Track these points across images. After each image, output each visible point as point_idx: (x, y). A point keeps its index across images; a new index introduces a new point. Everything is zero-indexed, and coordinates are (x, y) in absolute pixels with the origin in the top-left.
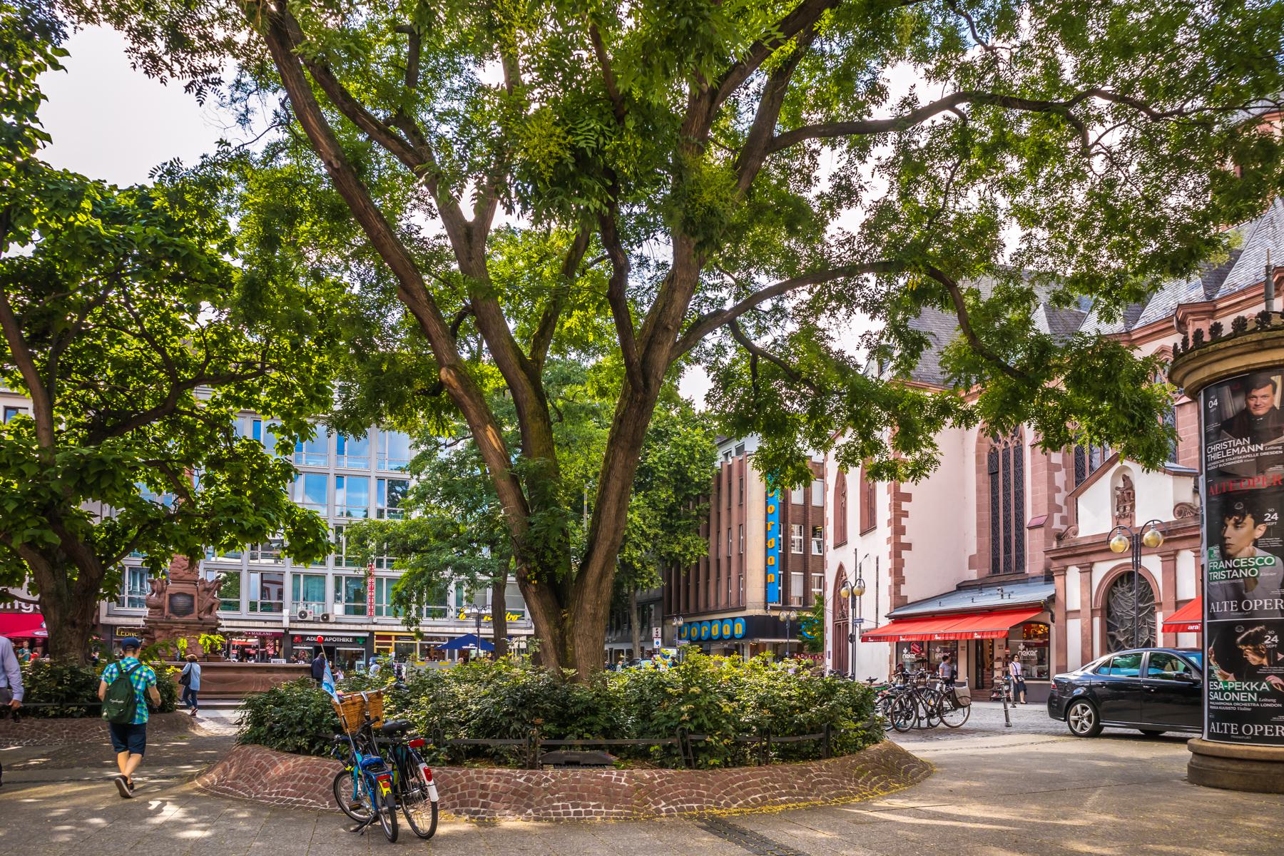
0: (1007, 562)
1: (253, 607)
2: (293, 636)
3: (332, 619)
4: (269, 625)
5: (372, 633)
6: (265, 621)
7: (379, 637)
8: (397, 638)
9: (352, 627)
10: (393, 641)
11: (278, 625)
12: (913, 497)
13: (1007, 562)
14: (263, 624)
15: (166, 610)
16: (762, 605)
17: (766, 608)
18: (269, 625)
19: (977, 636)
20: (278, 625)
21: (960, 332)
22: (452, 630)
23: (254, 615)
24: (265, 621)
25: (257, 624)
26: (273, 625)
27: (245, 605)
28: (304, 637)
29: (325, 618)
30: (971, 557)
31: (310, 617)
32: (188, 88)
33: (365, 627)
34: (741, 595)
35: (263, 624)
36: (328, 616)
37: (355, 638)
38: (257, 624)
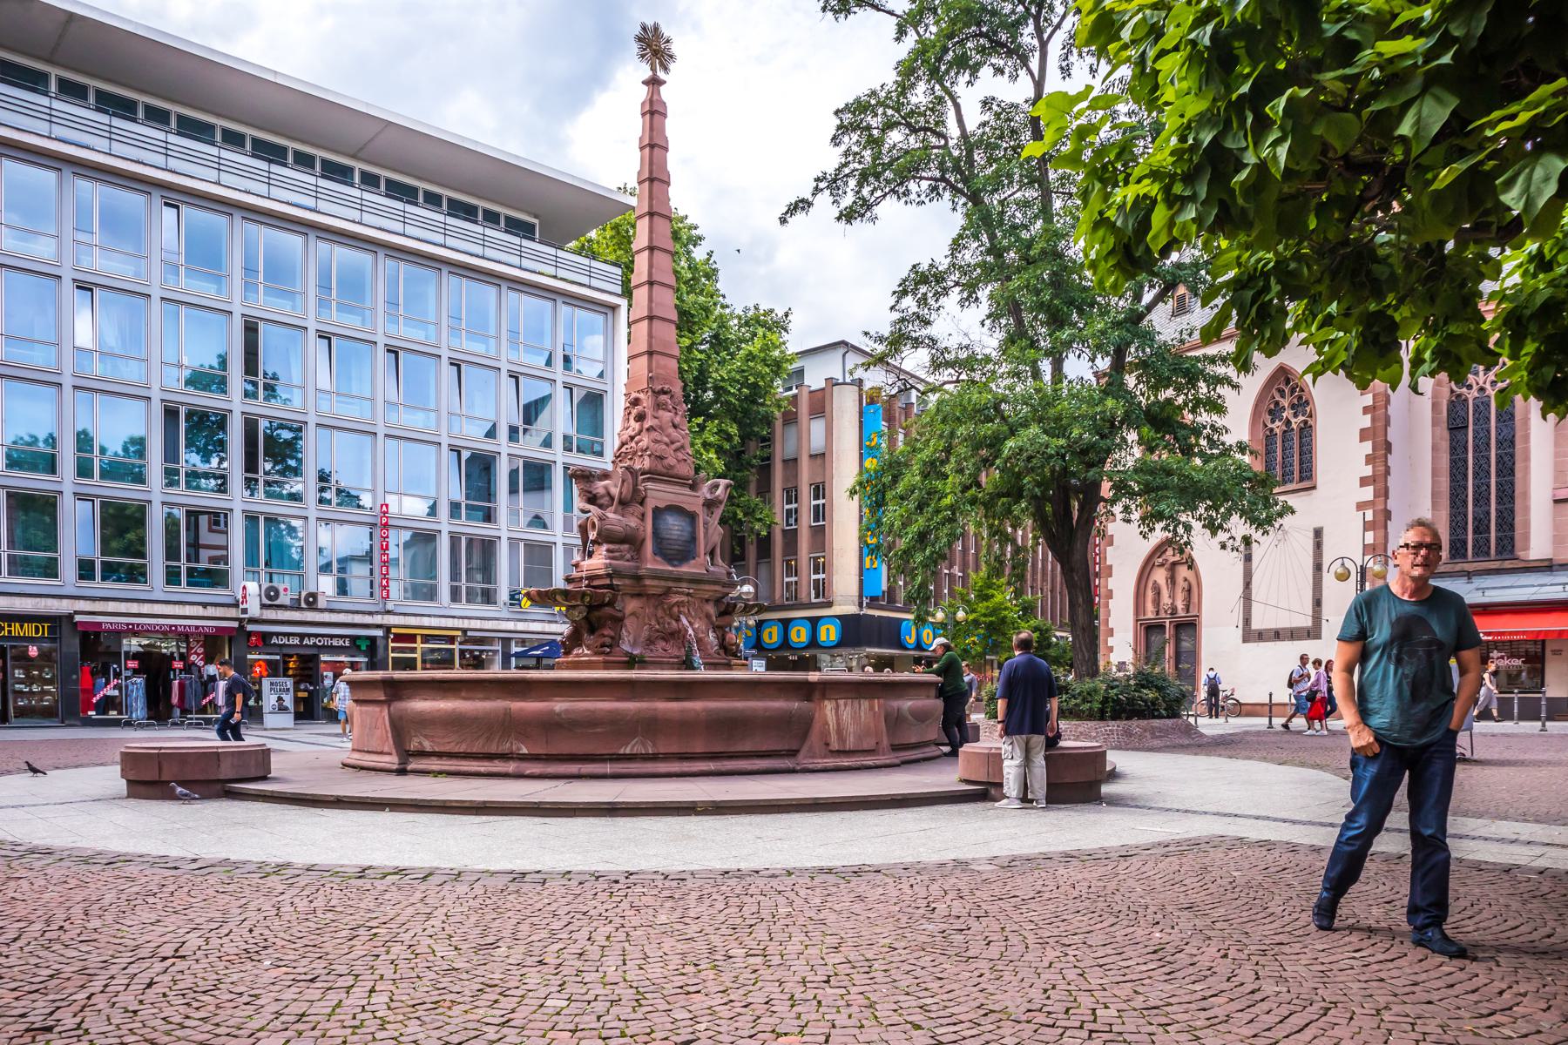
0: (1481, 527)
1: (86, 570)
2: (250, 634)
3: (321, 603)
4: (211, 611)
5: (388, 629)
6: (205, 605)
7: (399, 638)
8: (426, 639)
9: (358, 619)
10: (419, 645)
11: (232, 613)
12: (1318, 525)
13: (1481, 527)
14: (199, 611)
15: (649, 546)
16: (856, 599)
17: (861, 605)
18: (211, 611)
19: (921, 669)
20: (232, 613)
21: (865, 704)
22: (510, 626)
23: (88, 587)
24: (205, 605)
25: (188, 610)
26: (219, 612)
27: (68, 569)
28: (265, 637)
29: (312, 602)
30: (1362, 430)
31: (284, 599)
32: (1361, 506)
33: (378, 619)
34: (821, 588)
35: (199, 611)
36: (314, 595)
37: (354, 639)
38: (188, 610)
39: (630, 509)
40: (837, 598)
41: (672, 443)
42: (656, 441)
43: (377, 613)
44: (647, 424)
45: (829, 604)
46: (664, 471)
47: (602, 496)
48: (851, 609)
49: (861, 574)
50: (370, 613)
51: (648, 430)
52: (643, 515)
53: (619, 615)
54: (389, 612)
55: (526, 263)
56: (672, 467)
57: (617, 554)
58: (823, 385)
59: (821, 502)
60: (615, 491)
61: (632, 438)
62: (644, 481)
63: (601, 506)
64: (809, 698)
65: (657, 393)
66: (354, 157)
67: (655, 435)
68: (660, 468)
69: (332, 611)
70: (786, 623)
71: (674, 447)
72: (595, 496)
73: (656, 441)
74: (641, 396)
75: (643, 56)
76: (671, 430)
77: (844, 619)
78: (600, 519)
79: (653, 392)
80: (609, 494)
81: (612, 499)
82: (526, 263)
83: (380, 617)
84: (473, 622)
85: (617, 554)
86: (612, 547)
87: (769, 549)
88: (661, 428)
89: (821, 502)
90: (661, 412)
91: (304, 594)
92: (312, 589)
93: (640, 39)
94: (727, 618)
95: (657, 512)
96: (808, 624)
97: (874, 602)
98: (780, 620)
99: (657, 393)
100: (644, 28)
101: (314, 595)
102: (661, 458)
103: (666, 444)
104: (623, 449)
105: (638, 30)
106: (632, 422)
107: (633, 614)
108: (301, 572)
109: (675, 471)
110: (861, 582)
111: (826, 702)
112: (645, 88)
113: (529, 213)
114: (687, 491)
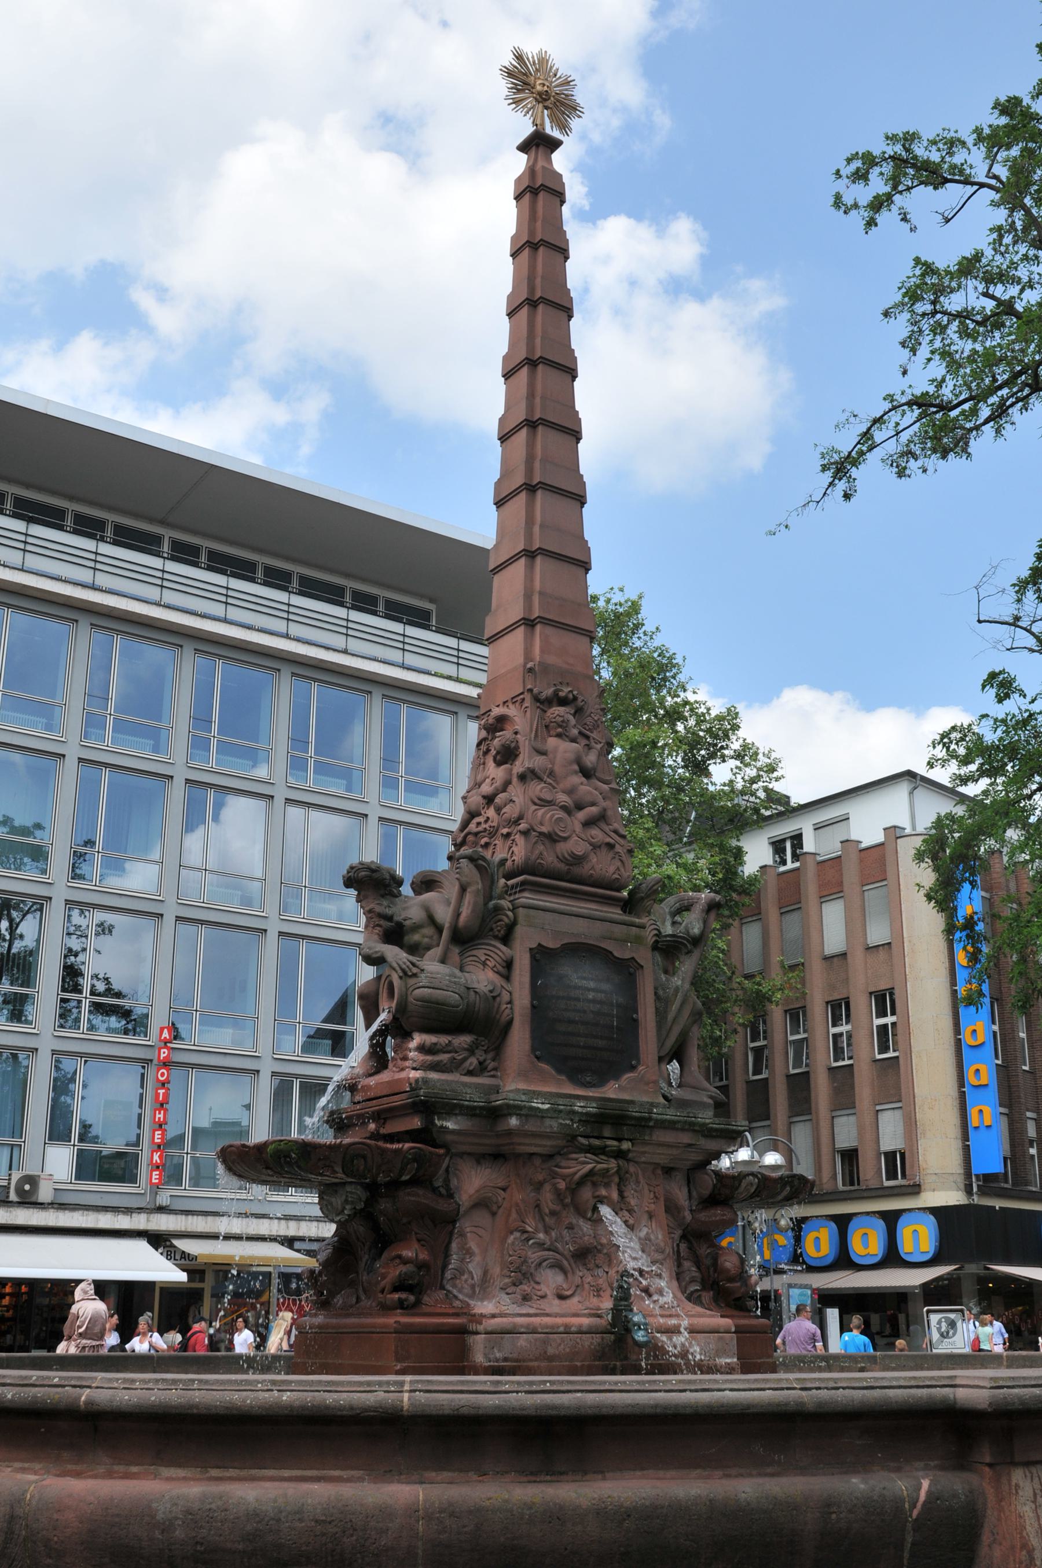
3: (45, 1194)
16: (961, 1180)
17: (968, 1190)
36: (32, 1180)
39: (481, 954)
40: (927, 1181)
41: (580, 807)
42: (543, 803)
43: (140, 1210)
44: (519, 766)
45: (915, 1190)
46: (563, 867)
47: (416, 928)
48: (952, 1197)
49: (965, 1137)
50: (128, 1211)
51: (522, 777)
52: (509, 965)
53: (442, 1205)
54: (161, 1209)
55: (411, 660)
56: (578, 860)
57: (444, 1057)
58: (880, 838)
59: (889, 1020)
60: (444, 915)
61: (489, 799)
62: (508, 891)
63: (414, 949)
64: (960, 1461)
65: (544, 703)
66: (163, 523)
67: (536, 789)
68: (550, 859)
69: (62, 1206)
70: (843, 1222)
71: (582, 815)
72: (400, 926)
73: (543, 803)
74: (512, 711)
75: (517, 102)
76: (578, 779)
77: (940, 1213)
78: (405, 975)
79: (536, 699)
80: (431, 919)
81: (439, 929)
82: (411, 660)
83: (143, 1217)
84: (304, 1225)
85: (444, 1057)
86: (430, 1039)
87: (807, 1100)
88: (551, 774)
89: (889, 1020)
90: (552, 742)
91: (16, 1176)
92: (31, 1169)
93: (510, 74)
94: (718, 1214)
95: (541, 957)
96: (881, 1224)
97: (989, 1183)
98: (834, 1218)
99: (544, 703)
100: (519, 57)
101: (32, 1180)
102: (552, 838)
103: (564, 808)
104: (472, 827)
105: (508, 60)
106: (491, 764)
107: (482, 1204)
108: (16, 1141)
109: (585, 870)
110: (966, 1150)
111: (1018, 1475)
112: (524, 157)
113: (421, 596)
114: (615, 913)
